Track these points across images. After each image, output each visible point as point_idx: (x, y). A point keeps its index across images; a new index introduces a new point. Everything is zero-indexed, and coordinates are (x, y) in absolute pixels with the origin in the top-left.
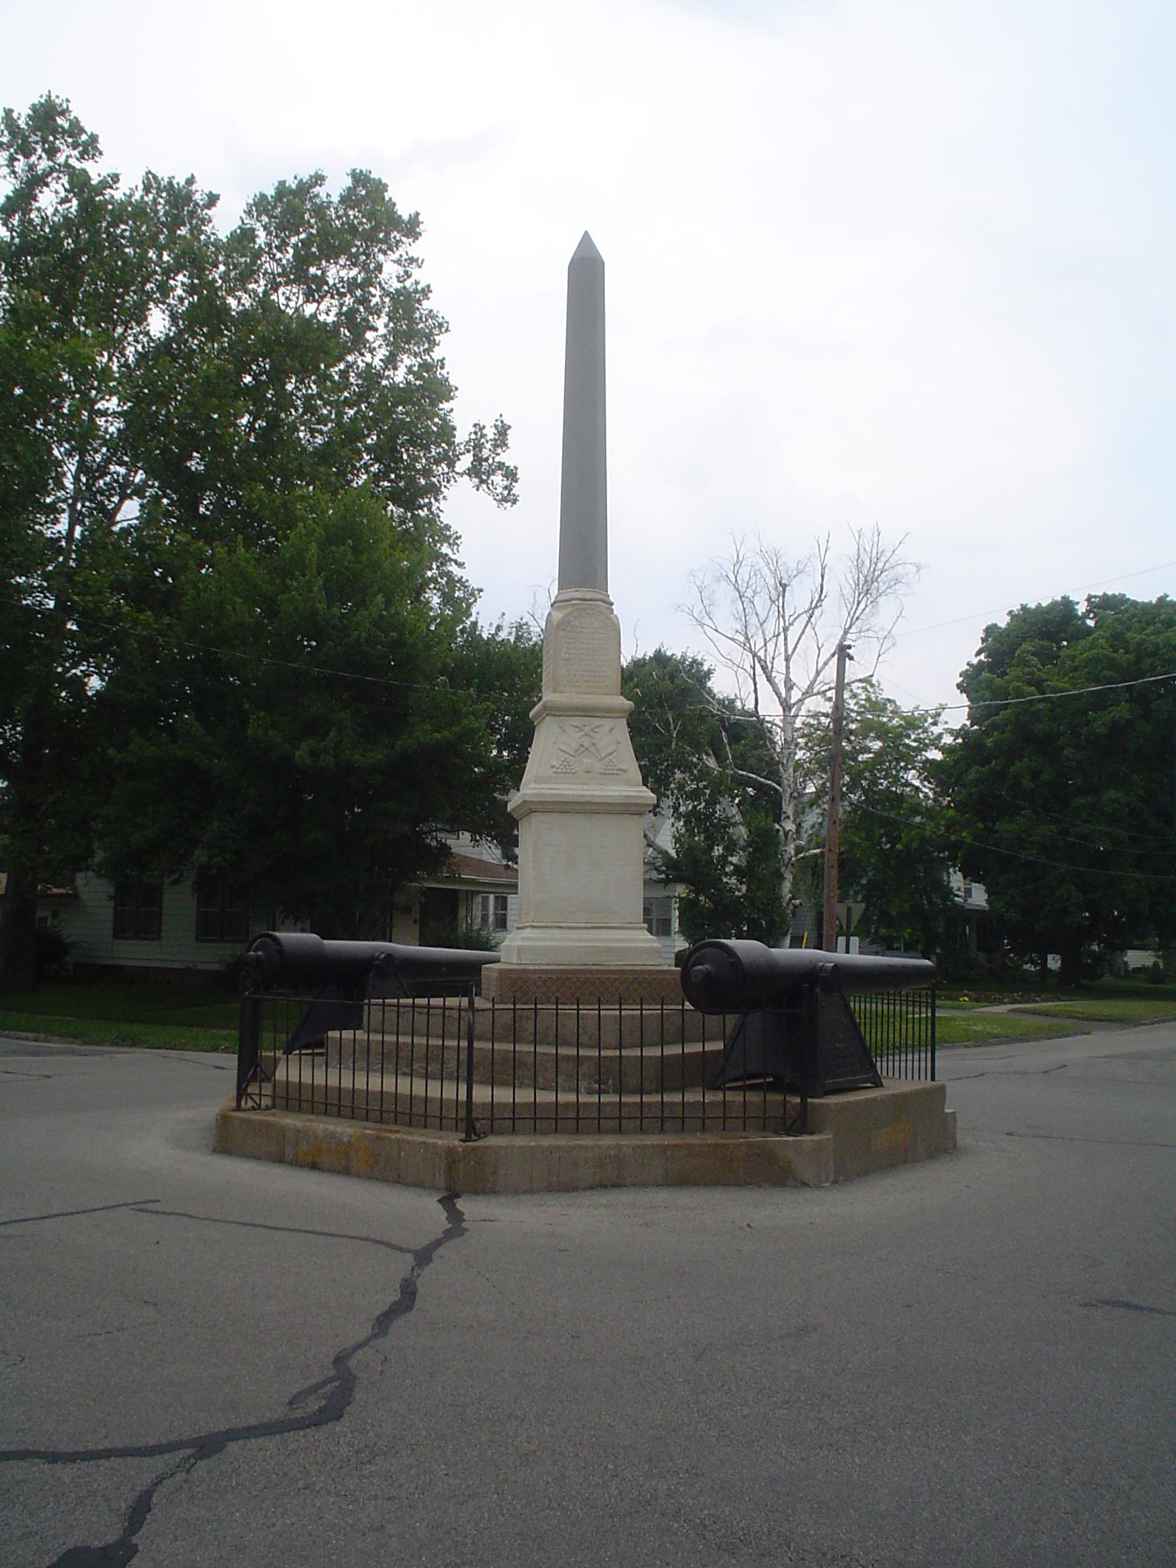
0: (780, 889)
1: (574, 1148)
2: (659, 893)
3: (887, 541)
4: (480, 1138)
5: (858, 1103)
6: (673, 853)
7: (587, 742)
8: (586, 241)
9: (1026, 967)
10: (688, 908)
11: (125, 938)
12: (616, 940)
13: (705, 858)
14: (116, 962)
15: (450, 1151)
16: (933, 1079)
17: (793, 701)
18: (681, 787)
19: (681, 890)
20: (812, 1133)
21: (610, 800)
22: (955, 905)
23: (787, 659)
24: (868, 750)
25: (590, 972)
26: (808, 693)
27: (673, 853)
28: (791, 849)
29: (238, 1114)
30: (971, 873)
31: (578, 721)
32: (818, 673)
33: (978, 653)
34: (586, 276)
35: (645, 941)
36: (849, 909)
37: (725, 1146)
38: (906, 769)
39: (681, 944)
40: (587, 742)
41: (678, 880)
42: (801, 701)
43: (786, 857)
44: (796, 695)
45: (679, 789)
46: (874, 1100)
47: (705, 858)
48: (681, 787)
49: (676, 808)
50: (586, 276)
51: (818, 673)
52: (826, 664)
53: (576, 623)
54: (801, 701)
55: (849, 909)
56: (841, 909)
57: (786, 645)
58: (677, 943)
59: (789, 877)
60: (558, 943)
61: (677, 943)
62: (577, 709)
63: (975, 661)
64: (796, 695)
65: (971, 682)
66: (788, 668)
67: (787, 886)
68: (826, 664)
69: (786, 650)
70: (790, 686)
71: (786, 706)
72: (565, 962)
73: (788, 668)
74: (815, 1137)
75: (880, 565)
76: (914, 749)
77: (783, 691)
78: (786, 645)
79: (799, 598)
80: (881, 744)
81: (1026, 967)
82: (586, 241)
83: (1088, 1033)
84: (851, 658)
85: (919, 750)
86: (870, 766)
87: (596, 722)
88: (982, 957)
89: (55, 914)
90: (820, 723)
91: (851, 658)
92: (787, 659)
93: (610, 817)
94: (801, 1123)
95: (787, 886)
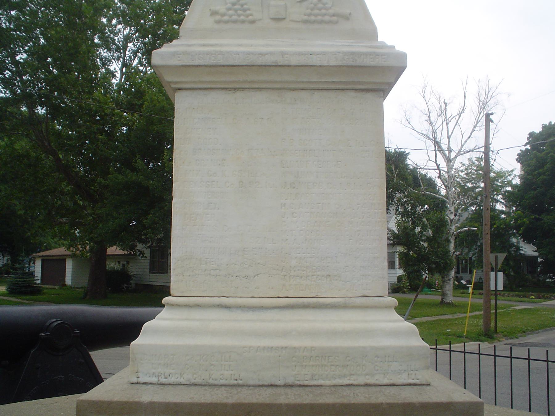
0: (449, 247)
2: (392, 250)
6: (396, 231)
9: (548, 280)
10: (404, 257)
11: (154, 273)
12: (334, 333)
13: (412, 233)
14: (151, 283)
17: (452, 158)
18: (399, 200)
19: (400, 249)
21: (315, 61)
22: (521, 254)
23: (449, 138)
24: (479, 187)
26: (459, 153)
27: (396, 231)
28: (453, 228)
30: (528, 239)
32: (462, 146)
33: (526, 145)
35: (395, 333)
36: (496, 257)
38: (497, 195)
39: (400, 272)
41: (399, 244)
42: (456, 157)
43: (451, 232)
44: (453, 155)
45: (398, 201)
47: (412, 233)
48: (399, 200)
49: (397, 210)
51: (462, 146)
52: (466, 142)
54: (456, 157)
55: (496, 257)
56: (492, 257)
57: (448, 131)
58: (398, 272)
59: (453, 241)
60: (216, 341)
61: (398, 272)
63: (523, 148)
64: (453, 155)
65: (522, 158)
66: (449, 142)
67: (452, 246)
68: (466, 142)
69: (448, 134)
70: (450, 151)
71: (449, 160)
73: (449, 142)
75: (490, 94)
76: (500, 186)
77: (447, 153)
78: (448, 131)
79: (453, 110)
81: (548, 280)
84: (492, 122)
85: (502, 187)
86: (480, 193)
88: (529, 276)
89: (128, 263)
90: (459, 175)
91: (492, 122)
92: (449, 138)
93: (317, 95)
95: (452, 246)
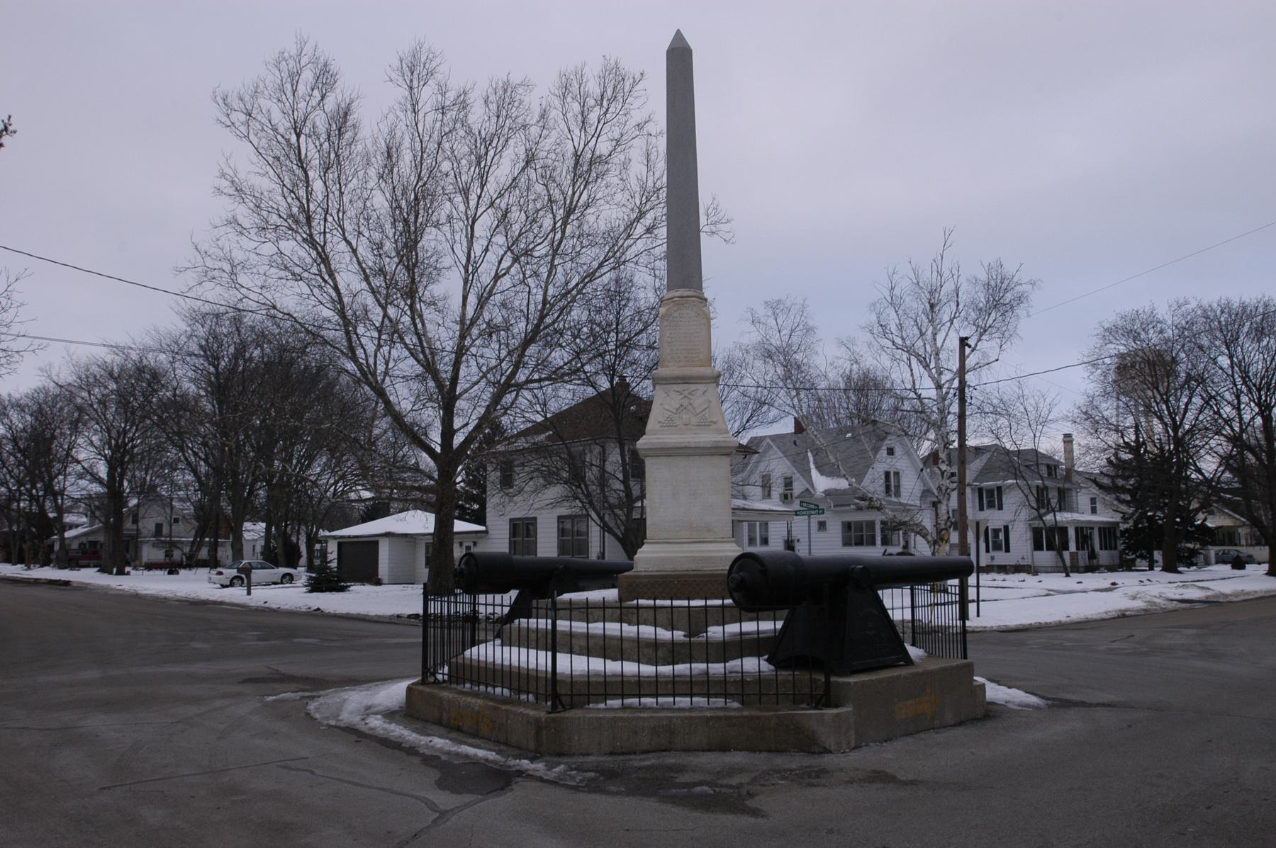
1: (634, 718)
3: (1009, 269)
4: (565, 710)
5: (880, 681)
7: (685, 402)
8: (678, 33)
15: (538, 720)
16: (965, 657)
20: (837, 706)
25: (689, 576)
29: (421, 688)
31: (680, 387)
34: (680, 59)
37: (758, 718)
40: (685, 402)
46: (898, 677)
50: (680, 59)
53: (676, 314)
62: (677, 378)
72: (668, 568)
74: (835, 711)
80: (1130, 456)
82: (678, 33)
83: (342, 589)
87: (694, 387)
94: (826, 699)
